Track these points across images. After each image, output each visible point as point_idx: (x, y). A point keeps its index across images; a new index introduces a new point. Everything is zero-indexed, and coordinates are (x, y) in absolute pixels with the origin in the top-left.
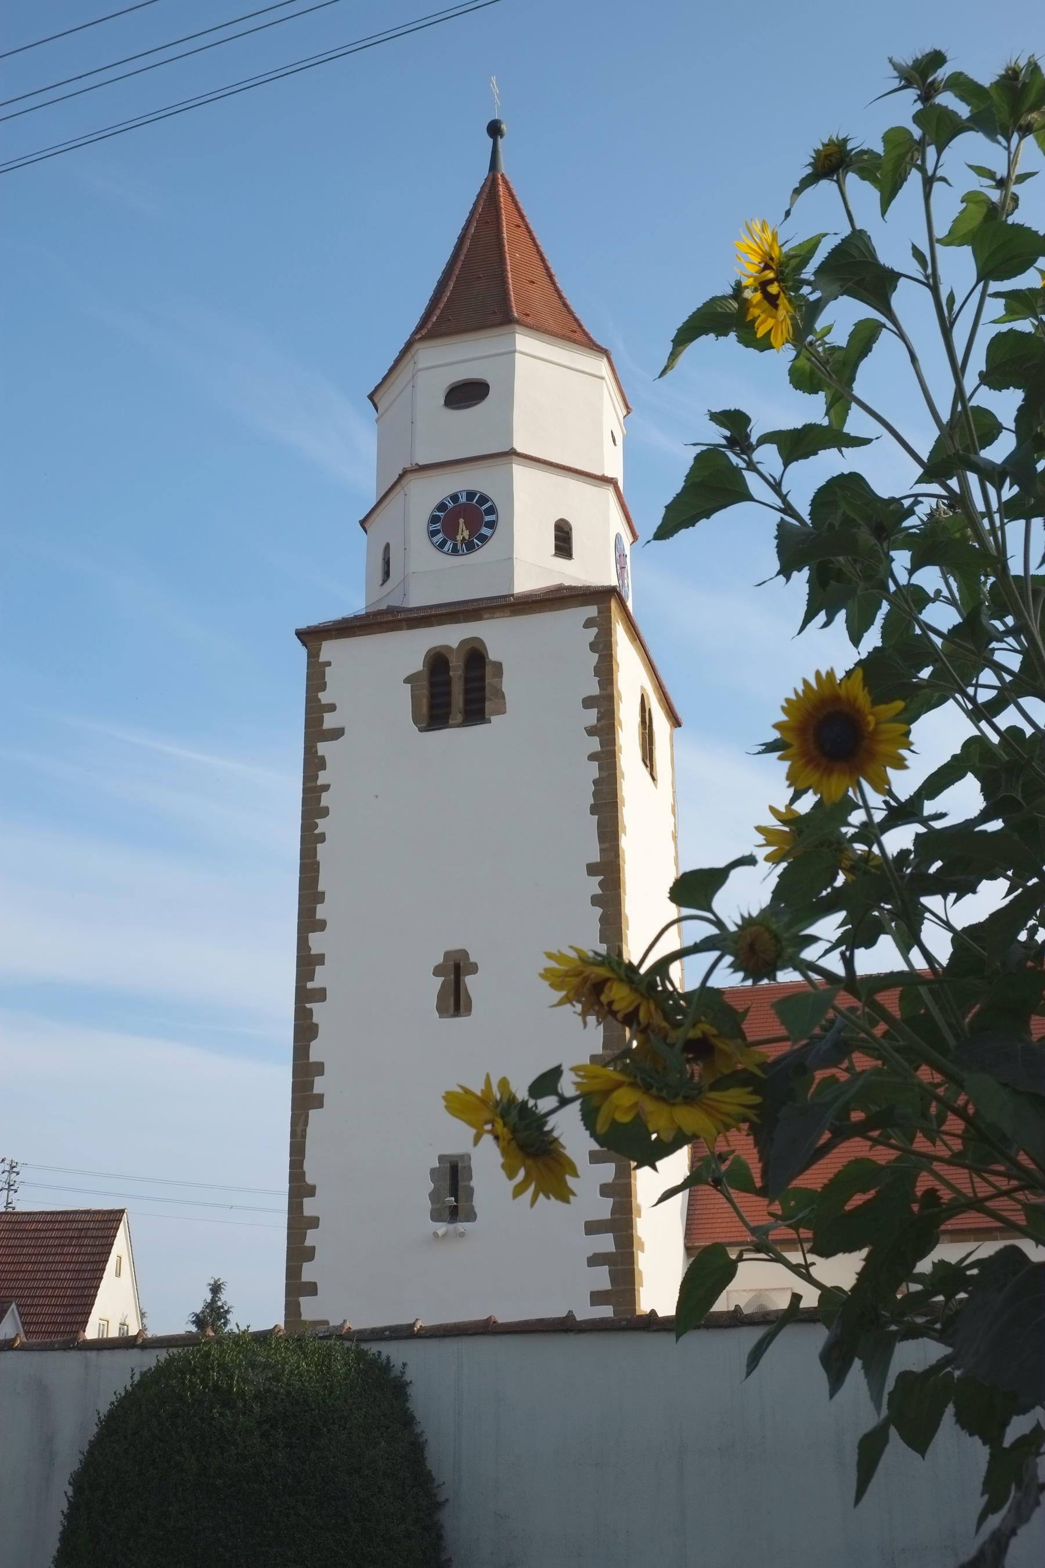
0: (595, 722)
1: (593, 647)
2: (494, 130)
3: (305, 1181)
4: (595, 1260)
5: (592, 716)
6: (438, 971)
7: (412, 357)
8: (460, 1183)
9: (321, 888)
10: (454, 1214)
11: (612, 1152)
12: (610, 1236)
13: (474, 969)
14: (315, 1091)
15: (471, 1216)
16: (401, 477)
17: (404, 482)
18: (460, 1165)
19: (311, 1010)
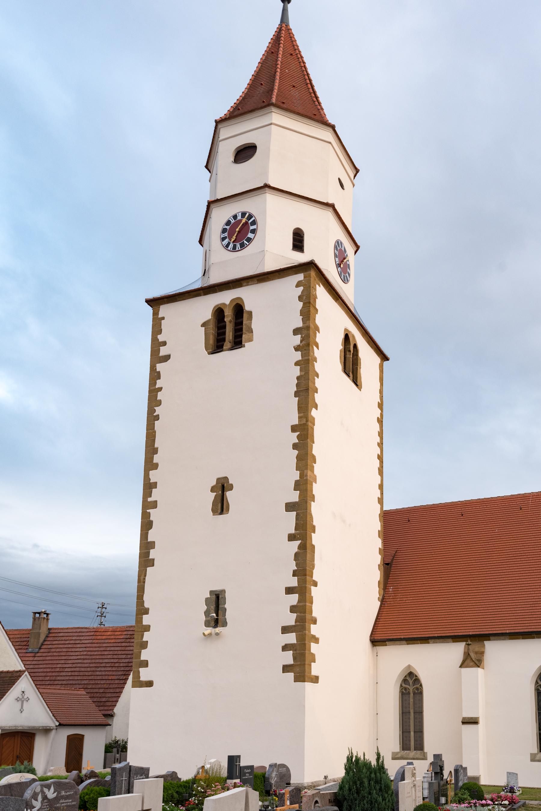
4: (285, 648)
6: (213, 490)
9: (156, 446)
15: (225, 624)
18: (220, 596)
19: (149, 513)
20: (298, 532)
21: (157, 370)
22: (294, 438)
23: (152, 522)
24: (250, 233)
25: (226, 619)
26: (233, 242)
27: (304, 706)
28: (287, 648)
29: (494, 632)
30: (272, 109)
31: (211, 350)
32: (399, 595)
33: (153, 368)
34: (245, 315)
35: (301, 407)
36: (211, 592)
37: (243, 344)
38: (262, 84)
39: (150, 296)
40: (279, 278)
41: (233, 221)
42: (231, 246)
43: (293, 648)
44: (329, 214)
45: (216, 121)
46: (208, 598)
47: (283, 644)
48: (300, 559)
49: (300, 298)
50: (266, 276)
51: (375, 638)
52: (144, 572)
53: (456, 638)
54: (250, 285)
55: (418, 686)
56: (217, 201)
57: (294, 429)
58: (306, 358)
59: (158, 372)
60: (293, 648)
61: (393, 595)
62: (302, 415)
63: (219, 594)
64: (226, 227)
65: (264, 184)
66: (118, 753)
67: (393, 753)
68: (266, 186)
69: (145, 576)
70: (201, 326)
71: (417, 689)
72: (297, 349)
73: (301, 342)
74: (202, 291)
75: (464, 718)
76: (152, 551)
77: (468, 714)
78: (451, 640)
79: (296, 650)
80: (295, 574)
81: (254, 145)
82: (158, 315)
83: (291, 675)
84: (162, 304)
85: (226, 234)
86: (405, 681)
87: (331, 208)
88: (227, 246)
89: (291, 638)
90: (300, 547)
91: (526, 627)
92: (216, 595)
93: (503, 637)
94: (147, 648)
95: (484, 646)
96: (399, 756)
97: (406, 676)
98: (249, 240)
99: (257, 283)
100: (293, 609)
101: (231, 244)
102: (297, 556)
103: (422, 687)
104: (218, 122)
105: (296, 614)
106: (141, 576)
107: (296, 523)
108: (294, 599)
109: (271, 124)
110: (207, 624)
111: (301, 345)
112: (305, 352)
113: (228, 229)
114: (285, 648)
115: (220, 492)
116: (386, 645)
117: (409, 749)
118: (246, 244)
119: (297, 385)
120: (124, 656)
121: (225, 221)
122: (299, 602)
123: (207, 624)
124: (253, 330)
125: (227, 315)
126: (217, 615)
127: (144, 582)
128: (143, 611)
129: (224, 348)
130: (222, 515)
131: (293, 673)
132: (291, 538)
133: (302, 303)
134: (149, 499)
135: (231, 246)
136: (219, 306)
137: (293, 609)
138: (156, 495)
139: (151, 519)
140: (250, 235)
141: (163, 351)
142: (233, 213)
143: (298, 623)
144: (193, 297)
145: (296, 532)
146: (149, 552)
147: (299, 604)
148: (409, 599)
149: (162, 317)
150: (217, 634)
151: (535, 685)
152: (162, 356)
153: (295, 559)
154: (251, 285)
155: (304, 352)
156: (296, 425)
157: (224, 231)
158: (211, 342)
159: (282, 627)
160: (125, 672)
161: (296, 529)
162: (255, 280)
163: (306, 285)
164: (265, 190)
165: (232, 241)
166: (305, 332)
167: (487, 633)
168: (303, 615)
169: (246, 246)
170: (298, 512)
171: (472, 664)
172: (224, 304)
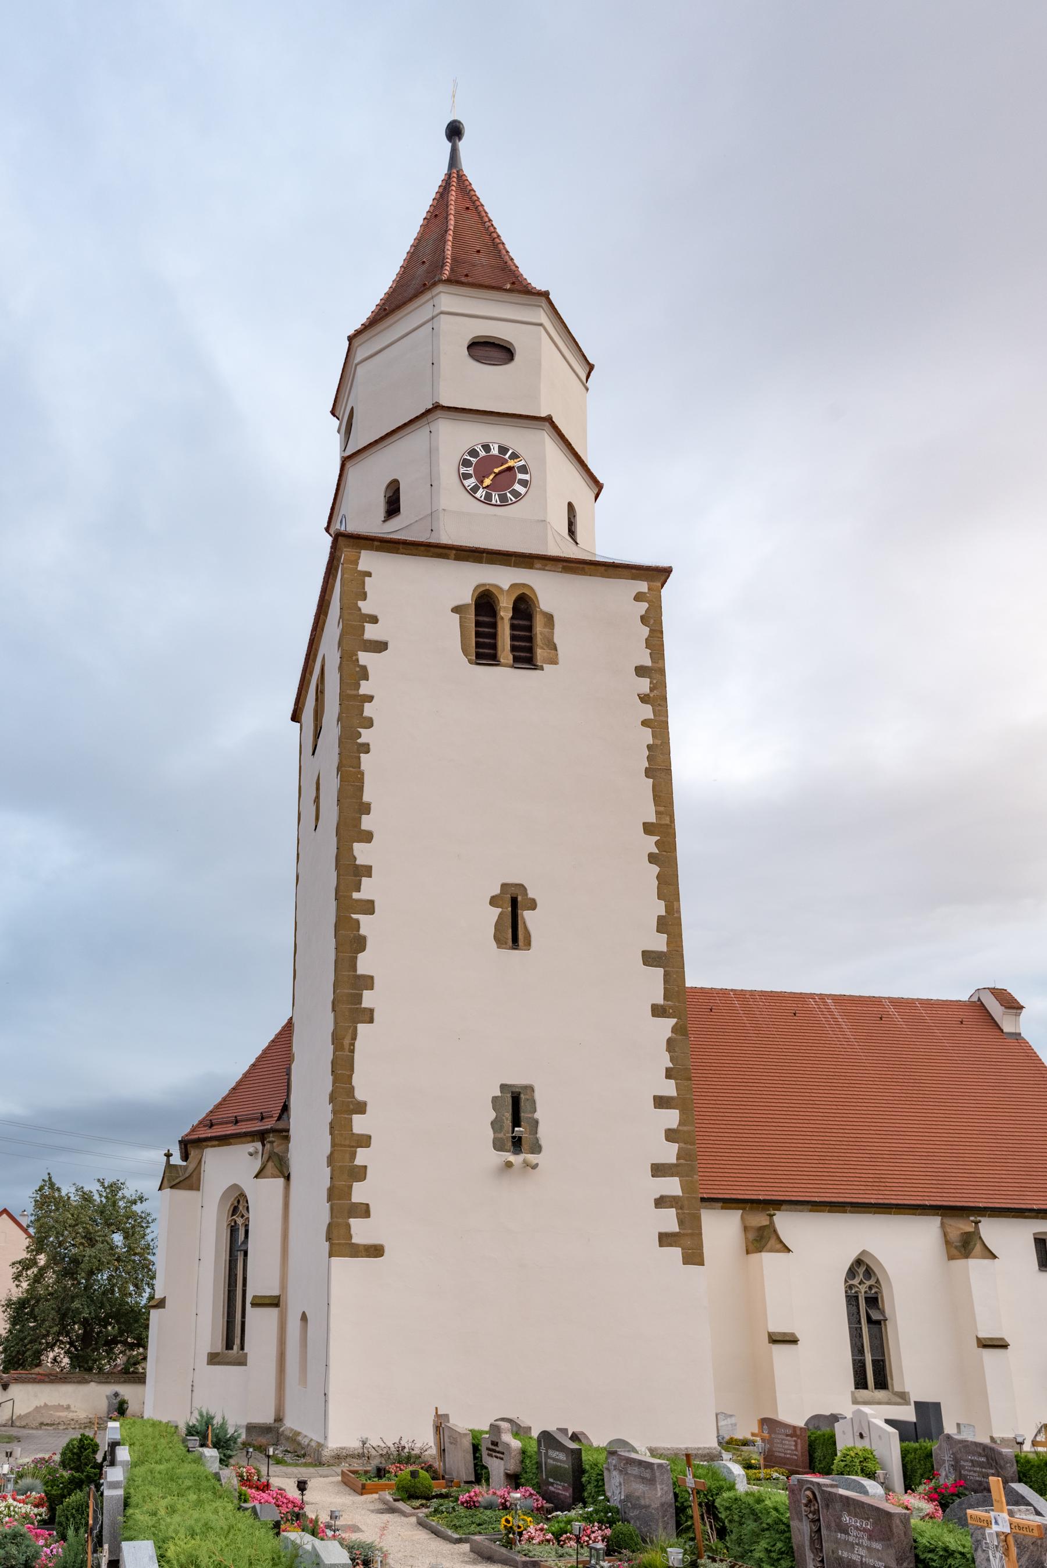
0: (648, 691)
1: (644, 619)
2: (454, 131)
3: (354, 1097)
4: (661, 1202)
5: (644, 685)
6: (494, 901)
7: (432, 298)
8: (522, 1114)
9: (366, 798)
10: (517, 1144)
11: (57, 1404)
12: (676, 1180)
13: (533, 905)
14: (364, 1005)
15: (536, 1148)
16: (428, 412)
17: (430, 417)
18: (522, 1096)
19: (358, 922)
20: (669, 1003)
25: (537, 1140)
36: (503, 1087)
42: (481, 493)
46: (498, 1097)
47: (658, 1196)
48: (677, 1049)
50: (581, 566)
52: (350, 1031)
60: (677, 1203)
63: (519, 1093)
64: (469, 458)
73: (651, 690)
76: (366, 993)
80: (669, 1074)
82: (357, 565)
83: (676, 1252)
85: (470, 470)
88: (475, 489)
90: (674, 1030)
94: (365, 1179)
99: (561, 572)
100: (671, 1135)
101: (481, 490)
107: (664, 988)
109: (541, 325)
110: (498, 1145)
111: (651, 695)
112: (660, 708)
114: (661, 1202)
115: (510, 909)
119: (649, 758)
121: (468, 446)
125: (505, 607)
127: (353, 1051)
128: (351, 1107)
131: (680, 1249)
134: (356, 895)
135: (481, 493)
136: (487, 587)
138: (368, 890)
139: (362, 932)
140: (517, 487)
143: (682, 1161)
144: (432, 557)
145: (666, 1002)
147: (681, 1128)
149: (366, 572)
151: (845, 1284)
155: (657, 708)
161: (665, 998)
162: (560, 565)
164: (544, 426)
170: (667, 969)
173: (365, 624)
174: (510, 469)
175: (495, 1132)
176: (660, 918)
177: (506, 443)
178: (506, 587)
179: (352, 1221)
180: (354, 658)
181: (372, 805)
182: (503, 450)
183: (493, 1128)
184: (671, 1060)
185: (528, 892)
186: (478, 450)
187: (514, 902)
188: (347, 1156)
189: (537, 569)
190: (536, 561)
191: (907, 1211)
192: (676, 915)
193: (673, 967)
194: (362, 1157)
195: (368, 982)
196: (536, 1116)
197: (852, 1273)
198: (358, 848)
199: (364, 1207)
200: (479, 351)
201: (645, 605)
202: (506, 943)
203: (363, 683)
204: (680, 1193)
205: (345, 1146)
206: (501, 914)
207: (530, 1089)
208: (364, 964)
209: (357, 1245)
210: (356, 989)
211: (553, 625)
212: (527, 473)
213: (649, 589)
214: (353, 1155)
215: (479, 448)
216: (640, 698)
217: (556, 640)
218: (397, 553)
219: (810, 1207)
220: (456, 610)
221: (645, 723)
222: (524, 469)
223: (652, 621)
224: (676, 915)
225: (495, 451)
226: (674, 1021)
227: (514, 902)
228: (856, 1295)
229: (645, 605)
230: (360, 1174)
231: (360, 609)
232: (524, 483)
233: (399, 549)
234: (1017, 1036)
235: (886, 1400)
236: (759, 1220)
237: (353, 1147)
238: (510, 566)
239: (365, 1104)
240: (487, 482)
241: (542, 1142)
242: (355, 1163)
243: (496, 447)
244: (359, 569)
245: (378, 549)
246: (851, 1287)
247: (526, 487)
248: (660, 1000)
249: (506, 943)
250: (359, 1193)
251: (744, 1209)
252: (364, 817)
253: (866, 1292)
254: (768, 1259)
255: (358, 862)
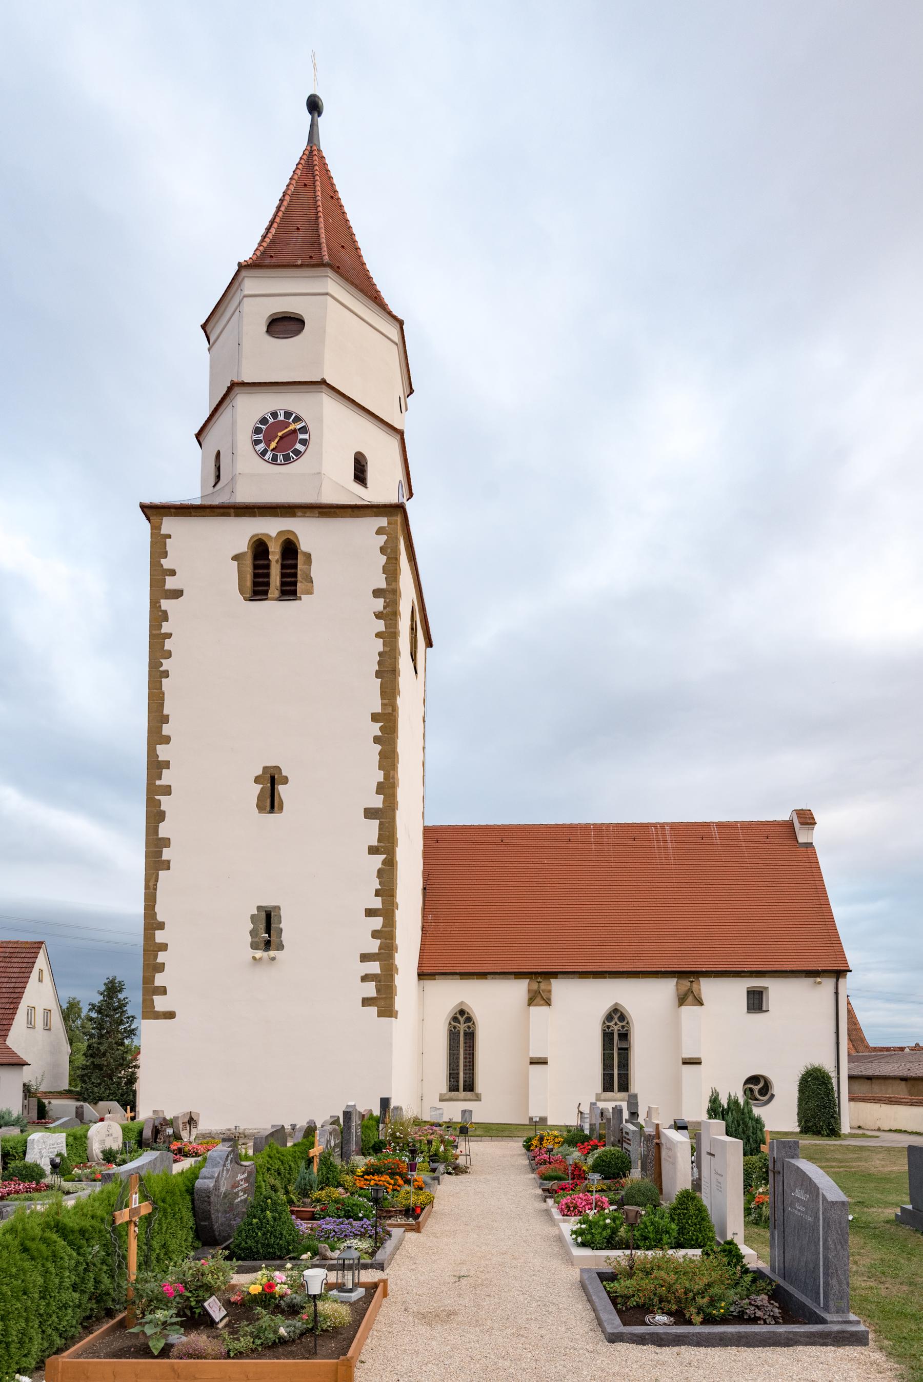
1: (383, 550)
2: (314, 106)
4: (365, 978)
5: (379, 604)
6: (257, 780)
9: (165, 712)
12: (377, 964)
13: (285, 781)
14: (163, 858)
15: (280, 947)
18: (273, 914)
19: (159, 801)
20: (382, 844)
21: (163, 608)
22: (375, 729)
23: (164, 812)
24: (299, 443)
25: (281, 941)
26: (272, 450)
27: (391, 1044)
28: (369, 978)
29: (564, 970)
30: (328, 273)
31: (248, 596)
32: (442, 924)
33: (155, 605)
34: (301, 559)
35: (386, 692)
36: (259, 908)
37: (298, 595)
38: (298, 229)
39: (147, 501)
40: (351, 516)
41: (271, 420)
42: (269, 455)
43: (376, 978)
44: (395, 443)
45: (239, 264)
46: (255, 915)
47: (363, 974)
48: (384, 876)
49: (383, 550)
50: (333, 510)
51: (425, 971)
52: (154, 876)
53: (519, 975)
54: (308, 517)
55: (470, 1024)
56: (243, 384)
57: (375, 717)
58: (392, 630)
59: (163, 611)
60: (376, 978)
61: (434, 924)
62: (386, 701)
63: (271, 912)
64: (260, 426)
65: (322, 379)
66: (26, 1099)
67: (441, 1095)
68: (323, 382)
69: (157, 881)
70: (232, 559)
71: (469, 1028)
72: (378, 616)
73: (385, 608)
74: (232, 510)
75: (531, 1058)
76: (165, 850)
77: (535, 1054)
78: (513, 976)
79: (379, 982)
80: (378, 893)
81: (301, 318)
82: (160, 530)
83: (373, 1010)
84: (167, 515)
85: (261, 437)
86: (455, 1019)
87: (399, 436)
88: (264, 453)
89: (374, 968)
90: (384, 863)
91: (598, 967)
92: (266, 911)
93: (572, 976)
94: (163, 971)
95: (550, 984)
96: (447, 1097)
97: (456, 1014)
98: (298, 453)
99: (318, 517)
100: (375, 934)
101: (269, 452)
102: (380, 873)
103: (475, 1026)
104: (241, 267)
105: (379, 940)
106: (149, 881)
107: (379, 834)
108: (377, 923)
109: (327, 294)
110: (254, 946)
111: (384, 612)
112: (391, 622)
113: (264, 430)
114: (365, 978)
115: (269, 785)
116: (486, 979)
117: (458, 1090)
118: (293, 458)
119: (379, 663)
120: (6, 980)
121: (259, 416)
122: (383, 926)
123: (254, 946)
124: (313, 579)
125: (272, 552)
126: (270, 937)
127: (156, 889)
128: (155, 926)
129: (269, 595)
130: (272, 814)
131: (376, 1008)
132: (373, 850)
133: (386, 557)
134: (158, 783)
135: (269, 455)
136: (260, 537)
137: (375, 934)
138: (167, 778)
139: (162, 808)
140: (299, 446)
141: (171, 583)
142: (273, 408)
143: (383, 951)
144: (217, 516)
145: (379, 844)
146: (162, 851)
147: (383, 929)
148: (454, 929)
149: (167, 535)
150: (273, 959)
151: (602, 1025)
152: (170, 590)
153: (378, 877)
154: (313, 517)
155: (388, 622)
156: (378, 714)
157: (257, 431)
158: (249, 583)
159: (361, 954)
160: (11, 999)
161: (379, 841)
162: (316, 511)
163: (392, 534)
164: (322, 388)
165: (271, 449)
166: (390, 596)
167: (556, 970)
168: (388, 941)
169: (292, 460)
170: (381, 820)
171: (542, 1002)
172: (268, 536)
173: (166, 577)
174: (294, 431)
175: (252, 938)
176: (379, 784)
177: (290, 408)
178: (274, 534)
179: (155, 997)
180: (158, 605)
181: (170, 717)
182: (288, 414)
183: (251, 935)
184: (380, 883)
185: (283, 772)
186: (268, 418)
187: (273, 780)
188: (152, 957)
189: (299, 517)
190: (296, 510)
191: (651, 975)
192: (391, 781)
193: (386, 819)
194: (162, 957)
195: (166, 842)
196: (281, 926)
197: (609, 1017)
198: (160, 748)
199: (163, 989)
200: (278, 327)
201: (384, 537)
202: (265, 809)
203: (164, 624)
204: (379, 972)
205: (150, 951)
206: (262, 788)
207: (278, 908)
208: (164, 830)
209: (158, 1012)
210: (158, 848)
211: (311, 562)
212: (306, 433)
213: (388, 524)
214: (156, 957)
215: (269, 416)
216: (375, 615)
217: (312, 575)
218: (191, 516)
219: (578, 976)
220: (235, 558)
221: (378, 635)
222: (304, 430)
223: (389, 550)
224: (391, 781)
225: (281, 417)
226: (384, 856)
227: (273, 780)
228: (626, 1032)
229: (384, 537)
230: (161, 968)
231: (162, 566)
232: (304, 442)
233: (191, 513)
234: (810, 845)
235: (621, 1098)
236: (685, 984)
237: (156, 951)
238: (279, 517)
239: (164, 923)
240: (273, 445)
241: (284, 943)
242: (157, 961)
243: (282, 413)
244: (161, 533)
245: (176, 515)
246: (608, 1027)
247: (305, 445)
248: (375, 843)
249: (265, 809)
250: (159, 980)
251: (531, 978)
252: (164, 726)
253: (619, 1030)
254: (688, 1011)
255: (160, 759)
